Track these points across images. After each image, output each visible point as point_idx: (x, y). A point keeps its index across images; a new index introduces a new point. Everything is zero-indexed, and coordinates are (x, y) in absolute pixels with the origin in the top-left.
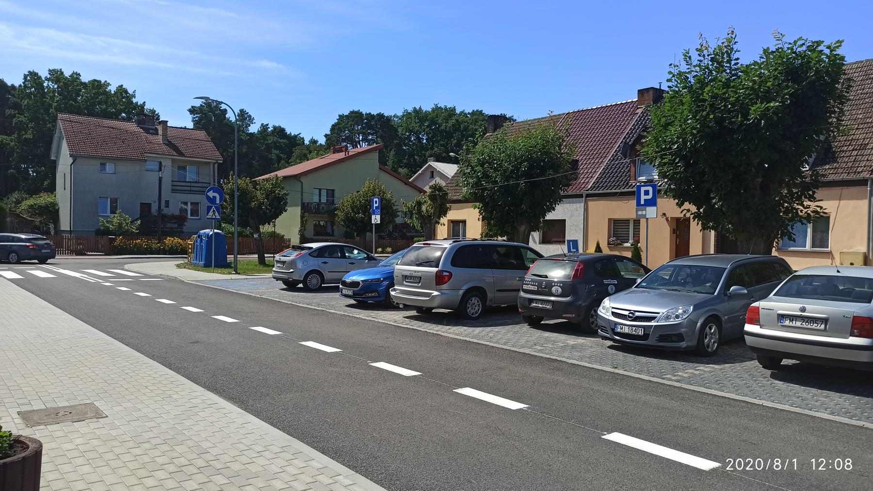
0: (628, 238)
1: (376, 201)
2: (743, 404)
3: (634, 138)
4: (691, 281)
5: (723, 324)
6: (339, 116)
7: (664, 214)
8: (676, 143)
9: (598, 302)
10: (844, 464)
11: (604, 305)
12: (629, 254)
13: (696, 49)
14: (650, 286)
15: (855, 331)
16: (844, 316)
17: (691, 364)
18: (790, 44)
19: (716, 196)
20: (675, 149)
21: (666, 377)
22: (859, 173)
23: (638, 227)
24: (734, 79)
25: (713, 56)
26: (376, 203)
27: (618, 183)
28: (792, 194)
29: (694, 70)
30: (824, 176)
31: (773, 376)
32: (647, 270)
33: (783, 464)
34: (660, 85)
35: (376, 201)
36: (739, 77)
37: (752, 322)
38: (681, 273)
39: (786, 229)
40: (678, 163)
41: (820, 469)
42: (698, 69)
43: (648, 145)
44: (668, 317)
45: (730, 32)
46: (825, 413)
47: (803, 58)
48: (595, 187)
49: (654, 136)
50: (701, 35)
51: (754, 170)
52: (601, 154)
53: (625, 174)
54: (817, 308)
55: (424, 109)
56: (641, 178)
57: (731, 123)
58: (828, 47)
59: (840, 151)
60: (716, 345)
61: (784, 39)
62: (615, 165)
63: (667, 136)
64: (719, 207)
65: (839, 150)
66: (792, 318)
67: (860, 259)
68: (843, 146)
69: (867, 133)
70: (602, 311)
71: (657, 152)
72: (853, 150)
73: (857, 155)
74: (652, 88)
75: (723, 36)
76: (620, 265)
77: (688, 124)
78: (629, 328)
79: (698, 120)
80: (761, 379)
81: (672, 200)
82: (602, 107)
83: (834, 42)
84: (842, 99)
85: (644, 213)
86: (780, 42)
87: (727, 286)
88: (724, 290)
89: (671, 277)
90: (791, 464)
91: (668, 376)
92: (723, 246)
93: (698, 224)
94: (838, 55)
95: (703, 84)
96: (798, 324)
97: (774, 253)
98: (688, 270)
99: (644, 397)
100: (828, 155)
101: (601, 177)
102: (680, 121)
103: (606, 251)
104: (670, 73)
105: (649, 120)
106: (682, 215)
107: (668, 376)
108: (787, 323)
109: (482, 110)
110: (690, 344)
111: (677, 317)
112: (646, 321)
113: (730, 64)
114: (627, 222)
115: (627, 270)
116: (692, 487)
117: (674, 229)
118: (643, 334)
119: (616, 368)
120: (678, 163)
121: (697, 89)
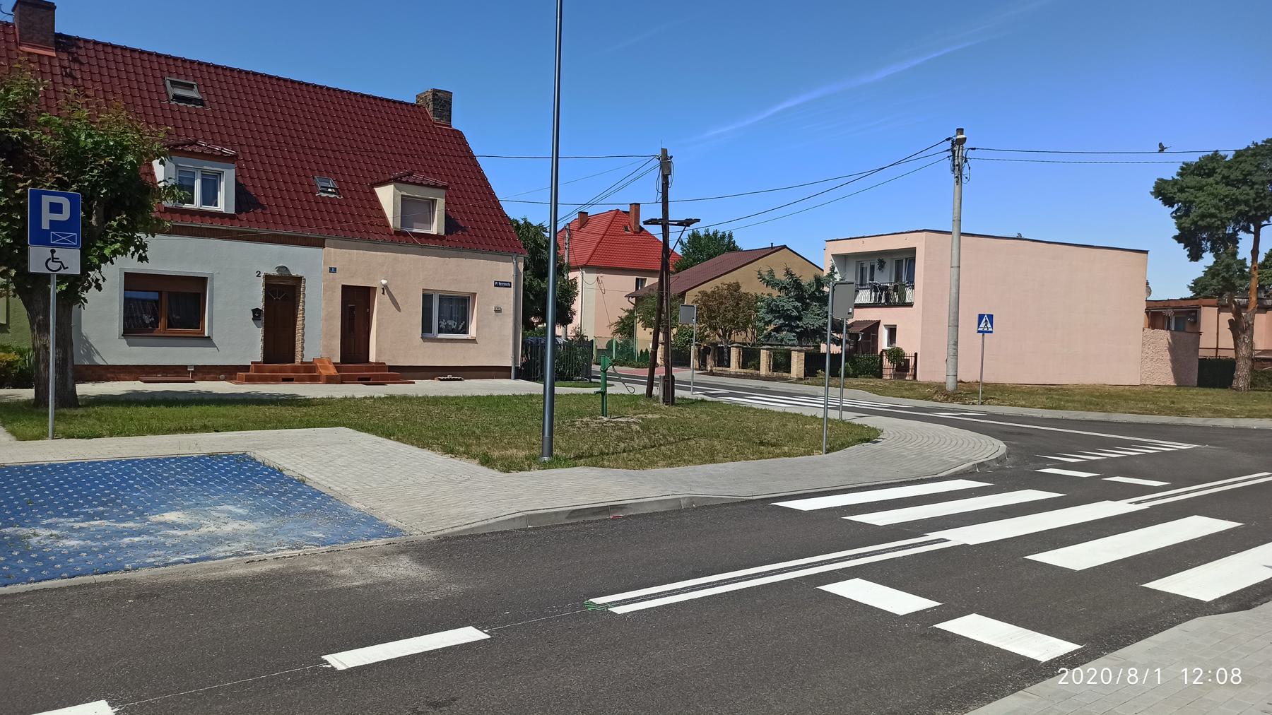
23: (1166, 327)
33: (1140, 675)
90: (1152, 676)
100: (541, 228)
114: (200, 294)
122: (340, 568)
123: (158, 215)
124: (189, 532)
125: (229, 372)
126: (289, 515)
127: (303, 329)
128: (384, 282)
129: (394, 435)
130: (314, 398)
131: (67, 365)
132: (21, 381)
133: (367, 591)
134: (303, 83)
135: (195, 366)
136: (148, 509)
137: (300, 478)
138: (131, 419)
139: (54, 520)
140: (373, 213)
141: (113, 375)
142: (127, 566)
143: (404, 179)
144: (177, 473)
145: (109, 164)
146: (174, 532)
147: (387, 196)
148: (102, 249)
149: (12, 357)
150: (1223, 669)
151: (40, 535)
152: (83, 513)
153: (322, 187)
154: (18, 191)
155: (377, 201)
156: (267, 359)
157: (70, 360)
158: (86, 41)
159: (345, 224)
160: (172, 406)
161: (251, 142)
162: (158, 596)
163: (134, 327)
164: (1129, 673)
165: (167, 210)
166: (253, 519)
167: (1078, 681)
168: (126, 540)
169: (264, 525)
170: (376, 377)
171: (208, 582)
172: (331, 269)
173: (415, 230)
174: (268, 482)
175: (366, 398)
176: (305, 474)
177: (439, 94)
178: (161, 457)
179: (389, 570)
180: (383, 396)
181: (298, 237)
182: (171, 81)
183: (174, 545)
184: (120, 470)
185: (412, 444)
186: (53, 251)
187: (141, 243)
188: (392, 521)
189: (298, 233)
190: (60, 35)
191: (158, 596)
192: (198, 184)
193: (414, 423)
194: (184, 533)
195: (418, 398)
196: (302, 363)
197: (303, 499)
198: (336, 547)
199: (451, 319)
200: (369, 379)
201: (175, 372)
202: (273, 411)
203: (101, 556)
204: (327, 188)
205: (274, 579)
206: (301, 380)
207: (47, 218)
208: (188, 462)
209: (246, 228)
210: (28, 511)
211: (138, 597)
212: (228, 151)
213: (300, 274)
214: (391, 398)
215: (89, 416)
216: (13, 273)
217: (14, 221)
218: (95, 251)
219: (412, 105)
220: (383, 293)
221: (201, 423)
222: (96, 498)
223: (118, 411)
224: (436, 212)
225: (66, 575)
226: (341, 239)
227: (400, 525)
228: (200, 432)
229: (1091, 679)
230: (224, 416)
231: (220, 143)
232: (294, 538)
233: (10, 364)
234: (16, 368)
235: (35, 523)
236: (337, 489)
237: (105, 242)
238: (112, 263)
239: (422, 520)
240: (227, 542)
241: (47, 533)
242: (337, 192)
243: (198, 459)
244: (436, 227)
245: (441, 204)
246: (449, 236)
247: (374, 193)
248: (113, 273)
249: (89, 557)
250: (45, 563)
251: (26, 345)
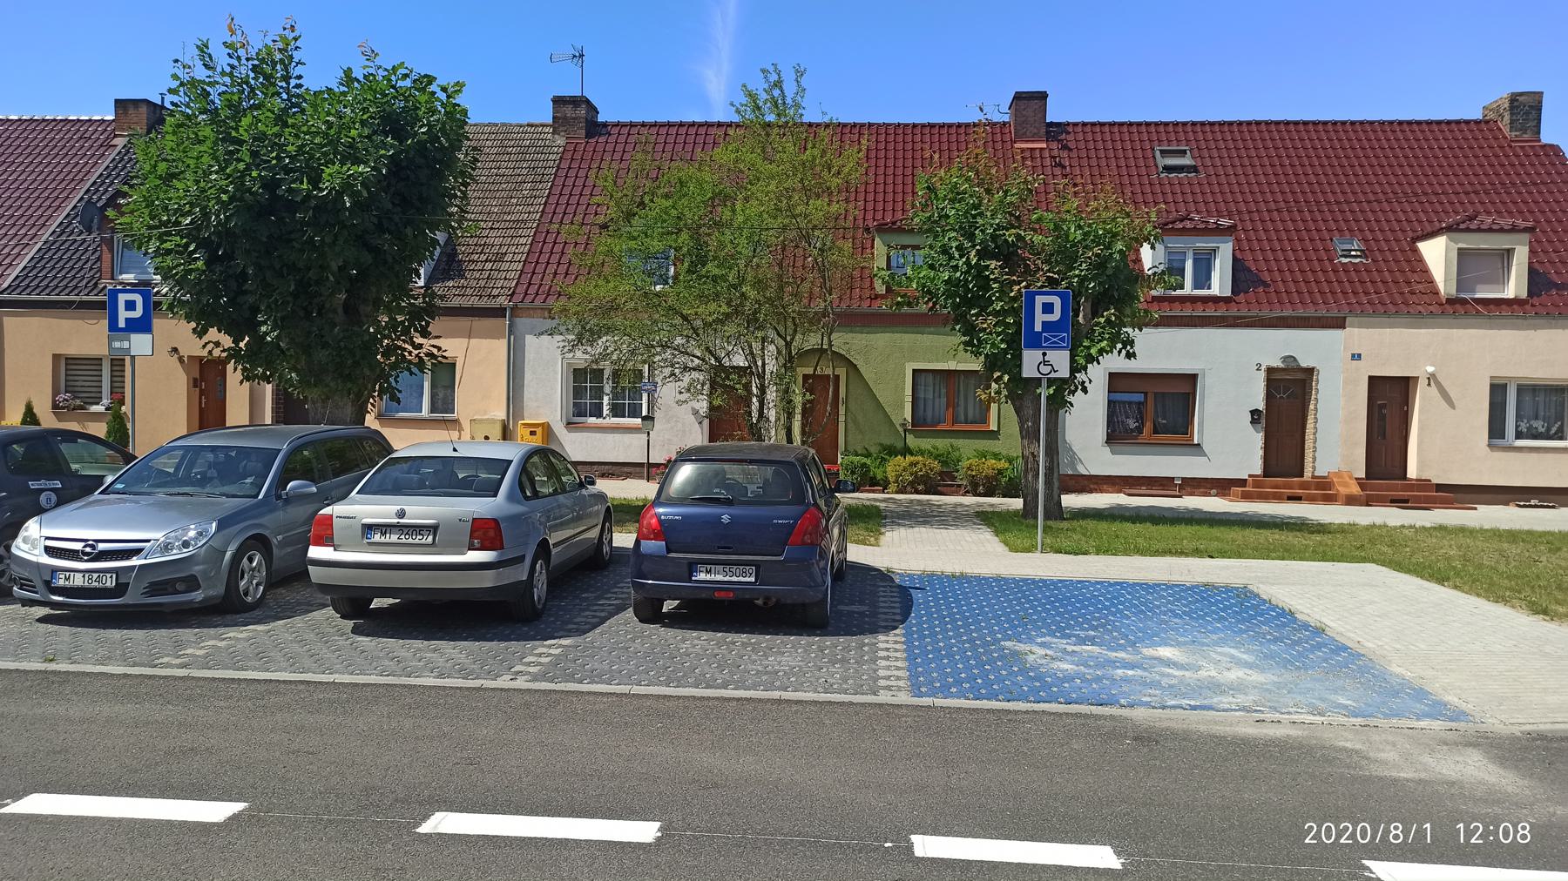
0: (98, 395)
2: (302, 687)
3: (108, 195)
4: (216, 475)
5: (275, 550)
7: (175, 350)
8: (189, 213)
9: (14, 529)
11: (26, 534)
12: (100, 430)
13: (223, 43)
14: (135, 489)
15: (476, 541)
16: (460, 520)
17: (212, 631)
18: (386, 70)
19: (268, 319)
20: (187, 225)
21: (161, 661)
22: (494, 297)
24: (294, 113)
25: (256, 62)
27: (74, 283)
28: (393, 325)
29: (221, 81)
30: (442, 297)
31: (356, 630)
32: (129, 458)
33: (1406, 832)
34: (163, 98)
36: (303, 111)
37: (321, 541)
38: (199, 461)
39: (387, 381)
40: (194, 251)
41: (1473, 841)
42: (227, 80)
43: (132, 212)
44: (166, 547)
45: (288, 26)
46: (430, 677)
47: (407, 100)
48: (18, 286)
49: (144, 196)
50: (232, 19)
51: (332, 278)
52: (33, 219)
53: (89, 265)
54: (421, 509)
56: (124, 276)
57: (290, 190)
58: (444, 89)
59: (469, 261)
60: (262, 588)
61: (378, 61)
62: (57, 245)
63: (170, 199)
64: (273, 339)
65: (467, 259)
66: (385, 528)
67: (497, 432)
68: (472, 254)
69: (504, 237)
70: (23, 546)
71: (150, 228)
72: (486, 261)
73: (491, 270)
75: (275, 31)
76: (65, 448)
77: (211, 181)
78: (84, 576)
79: (229, 176)
80: (336, 638)
81: (184, 322)
82: (32, 121)
83: (452, 84)
84: (465, 177)
85: (126, 345)
86: (372, 64)
87: (282, 481)
88: (277, 489)
89: (177, 468)
91: (165, 660)
92: (287, 410)
93: (235, 369)
94: (459, 105)
95: (237, 111)
96: (394, 538)
97: (371, 421)
98: (211, 456)
99: (106, 709)
101: (35, 267)
102: (196, 172)
103: (48, 421)
104: (175, 77)
105: (132, 163)
106: (205, 353)
107: (165, 660)
108: (377, 538)
110: (211, 593)
111: (186, 544)
112: (122, 559)
113: (288, 84)
114: (97, 361)
115: (80, 461)
116: (187, 861)
117: (195, 380)
118: (114, 584)
119: (51, 660)
120: (194, 251)
121: (227, 117)
122: (1379, 750)
123: (1145, 306)
124: (1187, 674)
125: (1222, 486)
126: (1306, 669)
127: (1314, 434)
128: (1430, 369)
129: (1448, 579)
130: (1330, 524)
131: (1053, 474)
132: (1010, 493)
133: (1420, 788)
134: (1225, 122)
135: (1183, 479)
136: (1142, 640)
137: (1319, 624)
138: (1117, 537)
139: (1048, 639)
140: (1414, 277)
141: (1096, 487)
142: (1123, 701)
143: (1462, 226)
144: (1169, 602)
145: (1097, 255)
146: (1170, 671)
147: (1436, 253)
148: (1088, 348)
149: (1003, 464)
151: (1036, 653)
152: (1075, 636)
153: (1343, 250)
154: (1012, 294)
155: (1421, 260)
156: (1267, 472)
157: (1056, 470)
158: (1076, 124)
159: (1374, 296)
160: (1181, 524)
161: (1356, 207)
162: (1157, 742)
163: (1117, 435)
164: (1519, 829)
165: (1154, 298)
166: (1263, 670)
168: (1120, 672)
169: (1275, 679)
170: (1418, 499)
171: (1213, 737)
172: (1353, 355)
173: (1478, 296)
174: (1277, 625)
175: (1403, 526)
176: (1324, 620)
177: (1521, 99)
178: (1150, 583)
179: (1452, 766)
180: (1429, 525)
181: (1309, 318)
182: (1161, 151)
183: (1171, 686)
184: (1109, 592)
185: (1478, 595)
186: (1044, 354)
187: (1128, 338)
188: (1451, 698)
189: (1310, 312)
190: (1052, 124)
191: (1157, 742)
192: (1189, 265)
193: (1480, 566)
194: (1181, 673)
195: (1482, 531)
196: (1314, 477)
197: (1323, 652)
198: (1372, 722)
199: (1536, 418)
200: (1407, 501)
201: (1161, 485)
202: (1277, 537)
203: (1094, 686)
204: (1349, 251)
205: (1293, 748)
206: (1312, 499)
207: (1040, 318)
208: (1182, 590)
209: (1244, 313)
210: (1022, 626)
211: (1135, 739)
212: (1225, 222)
213: (1312, 365)
214: (1441, 528)
215: (1075, 530)
216: (1006, 378)
217: (1007, 325)
218: (1082, 351)
219: (1477, 122)
220: (1429, 384)
221: (1194, 545)
222: (1088, 622)
223: (1103, 526)
224: (1514, 268)
225: (1062, 700)
226: (1369, 315)
227: (1464, 706)
228: (1192, 556)
229: (1310, 836)
230: (1217, 539)
231: (1215, 214)
232: (1314, 701)
233: (1000, 472)
234: (1006, 476)
235: (1031, 640)
236: (1370, 645)
237: (1092, 341)
238: (1099, 363)
239: (1501, 704)
240: (1231, 692)
241: (1041, 651)
242: (1364, 254)
243: (1192, 588)
244: (1514, 286)
245: (1521, 255)
246: (1535, 298)
247: (1416, 251)
248: (1097, 375)
249: (1083, 685)
250: (1042, 685)
251: (1016, 452)
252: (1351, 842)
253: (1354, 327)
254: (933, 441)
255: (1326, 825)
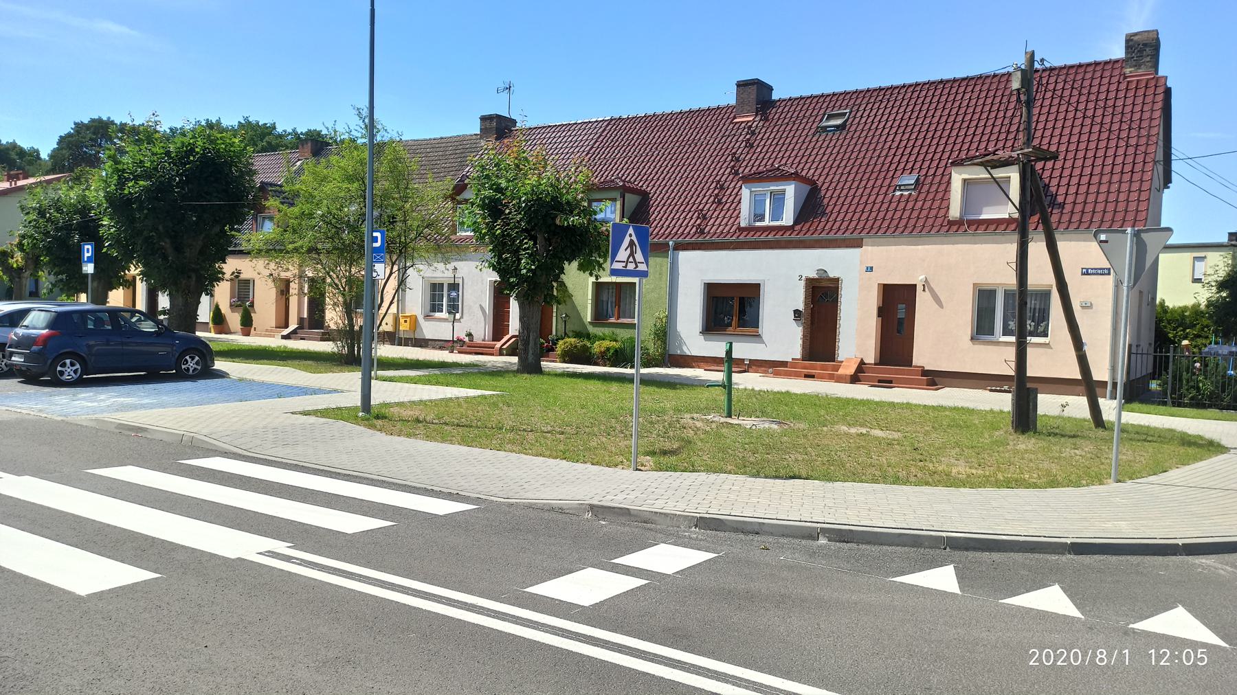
1: (88, 250)
6: (75, 124)
10: (1196, 656)
26: (88, 251)
33: (1109, 656)
35: (88, 250)
41: (1162, 663)
55: (226, 122)
74: (498, 117)
109: (321, 131)
135: (750, 360)
150: (1038, 653)
164: (1098, 654)
167: (1188, 662)
190: (1127, 53)
200: (891, 382)
220: (924, 290)
229: (1061, 660)
252: (1038, 664)
253: (868, 246)
254: (602, 329)
255: (1073, 651)
